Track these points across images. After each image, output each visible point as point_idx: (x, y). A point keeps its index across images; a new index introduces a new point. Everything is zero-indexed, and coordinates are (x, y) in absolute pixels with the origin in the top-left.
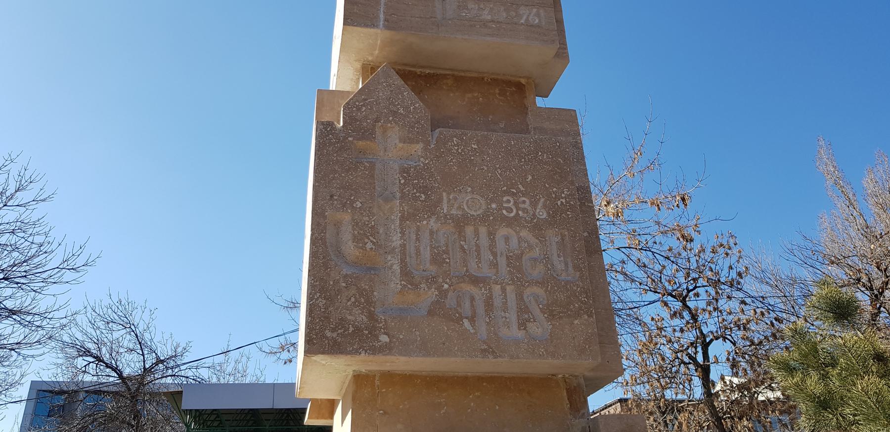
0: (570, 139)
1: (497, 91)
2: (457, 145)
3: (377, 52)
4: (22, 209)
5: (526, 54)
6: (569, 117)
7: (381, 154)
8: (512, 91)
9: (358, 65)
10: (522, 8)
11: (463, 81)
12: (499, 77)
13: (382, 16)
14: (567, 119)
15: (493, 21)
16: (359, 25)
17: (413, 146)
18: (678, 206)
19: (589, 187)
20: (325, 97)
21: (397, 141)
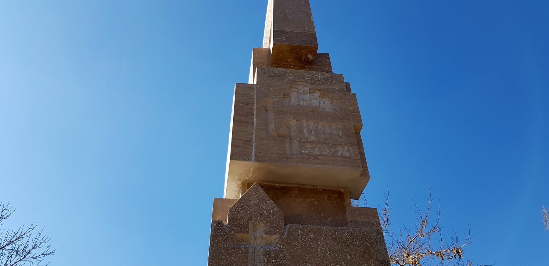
0: (374, 228)
1: (326, 197)
2: (301, 235)
3: (251, 175)
4: (35, 260)
5: (343, 175)
6: (372, 213)
7: (253, 242)
8: (336, 197)
9: (240, 182)
10: (339, 146)
11: (305, 191)
12: (327, 188)
13: (253, 154)
14: (371, 214)
15: (321, 155)
16: (239, 160)
17: (273, 236)
18: (455, 256)
19: (388, 261)
20: (219, 203)
21: (263, 233)
